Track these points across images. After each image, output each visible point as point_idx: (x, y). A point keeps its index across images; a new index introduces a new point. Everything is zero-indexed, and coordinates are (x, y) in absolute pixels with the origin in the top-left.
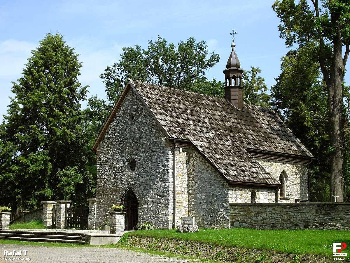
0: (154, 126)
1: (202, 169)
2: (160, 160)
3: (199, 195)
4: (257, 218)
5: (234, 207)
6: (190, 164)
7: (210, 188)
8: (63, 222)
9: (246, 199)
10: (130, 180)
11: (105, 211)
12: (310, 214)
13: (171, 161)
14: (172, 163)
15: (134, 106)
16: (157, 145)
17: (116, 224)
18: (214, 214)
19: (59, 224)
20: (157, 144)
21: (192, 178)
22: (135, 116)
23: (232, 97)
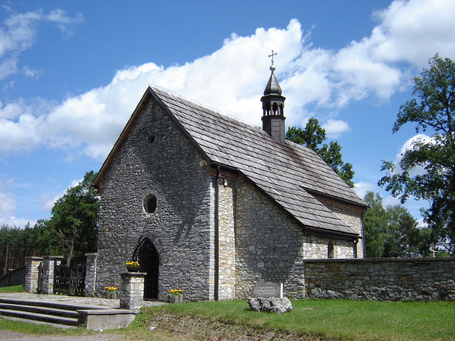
0: (186, 148)
1: (257, 209)
2: (194, 196)
3: (252, 248)
4: (353, 283)
5: (311, 265)
6: (237, 203)
7: (270, 236)
8: (51, 285)
9: (322, 254)
10: (148, 226)
11: (110, 270)
12: (451, 275)
13: (212, 197)
14: (214, 200)
15: (156, 123)
16: (190, 174)
17: (132, 292)
18: (277, 276)
19: (46, 288)
20: (190, 172)
21: (241, 224)
22: (157, 136)
23: (273, 129)
